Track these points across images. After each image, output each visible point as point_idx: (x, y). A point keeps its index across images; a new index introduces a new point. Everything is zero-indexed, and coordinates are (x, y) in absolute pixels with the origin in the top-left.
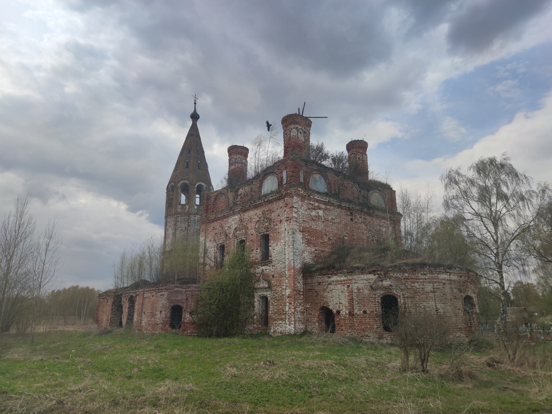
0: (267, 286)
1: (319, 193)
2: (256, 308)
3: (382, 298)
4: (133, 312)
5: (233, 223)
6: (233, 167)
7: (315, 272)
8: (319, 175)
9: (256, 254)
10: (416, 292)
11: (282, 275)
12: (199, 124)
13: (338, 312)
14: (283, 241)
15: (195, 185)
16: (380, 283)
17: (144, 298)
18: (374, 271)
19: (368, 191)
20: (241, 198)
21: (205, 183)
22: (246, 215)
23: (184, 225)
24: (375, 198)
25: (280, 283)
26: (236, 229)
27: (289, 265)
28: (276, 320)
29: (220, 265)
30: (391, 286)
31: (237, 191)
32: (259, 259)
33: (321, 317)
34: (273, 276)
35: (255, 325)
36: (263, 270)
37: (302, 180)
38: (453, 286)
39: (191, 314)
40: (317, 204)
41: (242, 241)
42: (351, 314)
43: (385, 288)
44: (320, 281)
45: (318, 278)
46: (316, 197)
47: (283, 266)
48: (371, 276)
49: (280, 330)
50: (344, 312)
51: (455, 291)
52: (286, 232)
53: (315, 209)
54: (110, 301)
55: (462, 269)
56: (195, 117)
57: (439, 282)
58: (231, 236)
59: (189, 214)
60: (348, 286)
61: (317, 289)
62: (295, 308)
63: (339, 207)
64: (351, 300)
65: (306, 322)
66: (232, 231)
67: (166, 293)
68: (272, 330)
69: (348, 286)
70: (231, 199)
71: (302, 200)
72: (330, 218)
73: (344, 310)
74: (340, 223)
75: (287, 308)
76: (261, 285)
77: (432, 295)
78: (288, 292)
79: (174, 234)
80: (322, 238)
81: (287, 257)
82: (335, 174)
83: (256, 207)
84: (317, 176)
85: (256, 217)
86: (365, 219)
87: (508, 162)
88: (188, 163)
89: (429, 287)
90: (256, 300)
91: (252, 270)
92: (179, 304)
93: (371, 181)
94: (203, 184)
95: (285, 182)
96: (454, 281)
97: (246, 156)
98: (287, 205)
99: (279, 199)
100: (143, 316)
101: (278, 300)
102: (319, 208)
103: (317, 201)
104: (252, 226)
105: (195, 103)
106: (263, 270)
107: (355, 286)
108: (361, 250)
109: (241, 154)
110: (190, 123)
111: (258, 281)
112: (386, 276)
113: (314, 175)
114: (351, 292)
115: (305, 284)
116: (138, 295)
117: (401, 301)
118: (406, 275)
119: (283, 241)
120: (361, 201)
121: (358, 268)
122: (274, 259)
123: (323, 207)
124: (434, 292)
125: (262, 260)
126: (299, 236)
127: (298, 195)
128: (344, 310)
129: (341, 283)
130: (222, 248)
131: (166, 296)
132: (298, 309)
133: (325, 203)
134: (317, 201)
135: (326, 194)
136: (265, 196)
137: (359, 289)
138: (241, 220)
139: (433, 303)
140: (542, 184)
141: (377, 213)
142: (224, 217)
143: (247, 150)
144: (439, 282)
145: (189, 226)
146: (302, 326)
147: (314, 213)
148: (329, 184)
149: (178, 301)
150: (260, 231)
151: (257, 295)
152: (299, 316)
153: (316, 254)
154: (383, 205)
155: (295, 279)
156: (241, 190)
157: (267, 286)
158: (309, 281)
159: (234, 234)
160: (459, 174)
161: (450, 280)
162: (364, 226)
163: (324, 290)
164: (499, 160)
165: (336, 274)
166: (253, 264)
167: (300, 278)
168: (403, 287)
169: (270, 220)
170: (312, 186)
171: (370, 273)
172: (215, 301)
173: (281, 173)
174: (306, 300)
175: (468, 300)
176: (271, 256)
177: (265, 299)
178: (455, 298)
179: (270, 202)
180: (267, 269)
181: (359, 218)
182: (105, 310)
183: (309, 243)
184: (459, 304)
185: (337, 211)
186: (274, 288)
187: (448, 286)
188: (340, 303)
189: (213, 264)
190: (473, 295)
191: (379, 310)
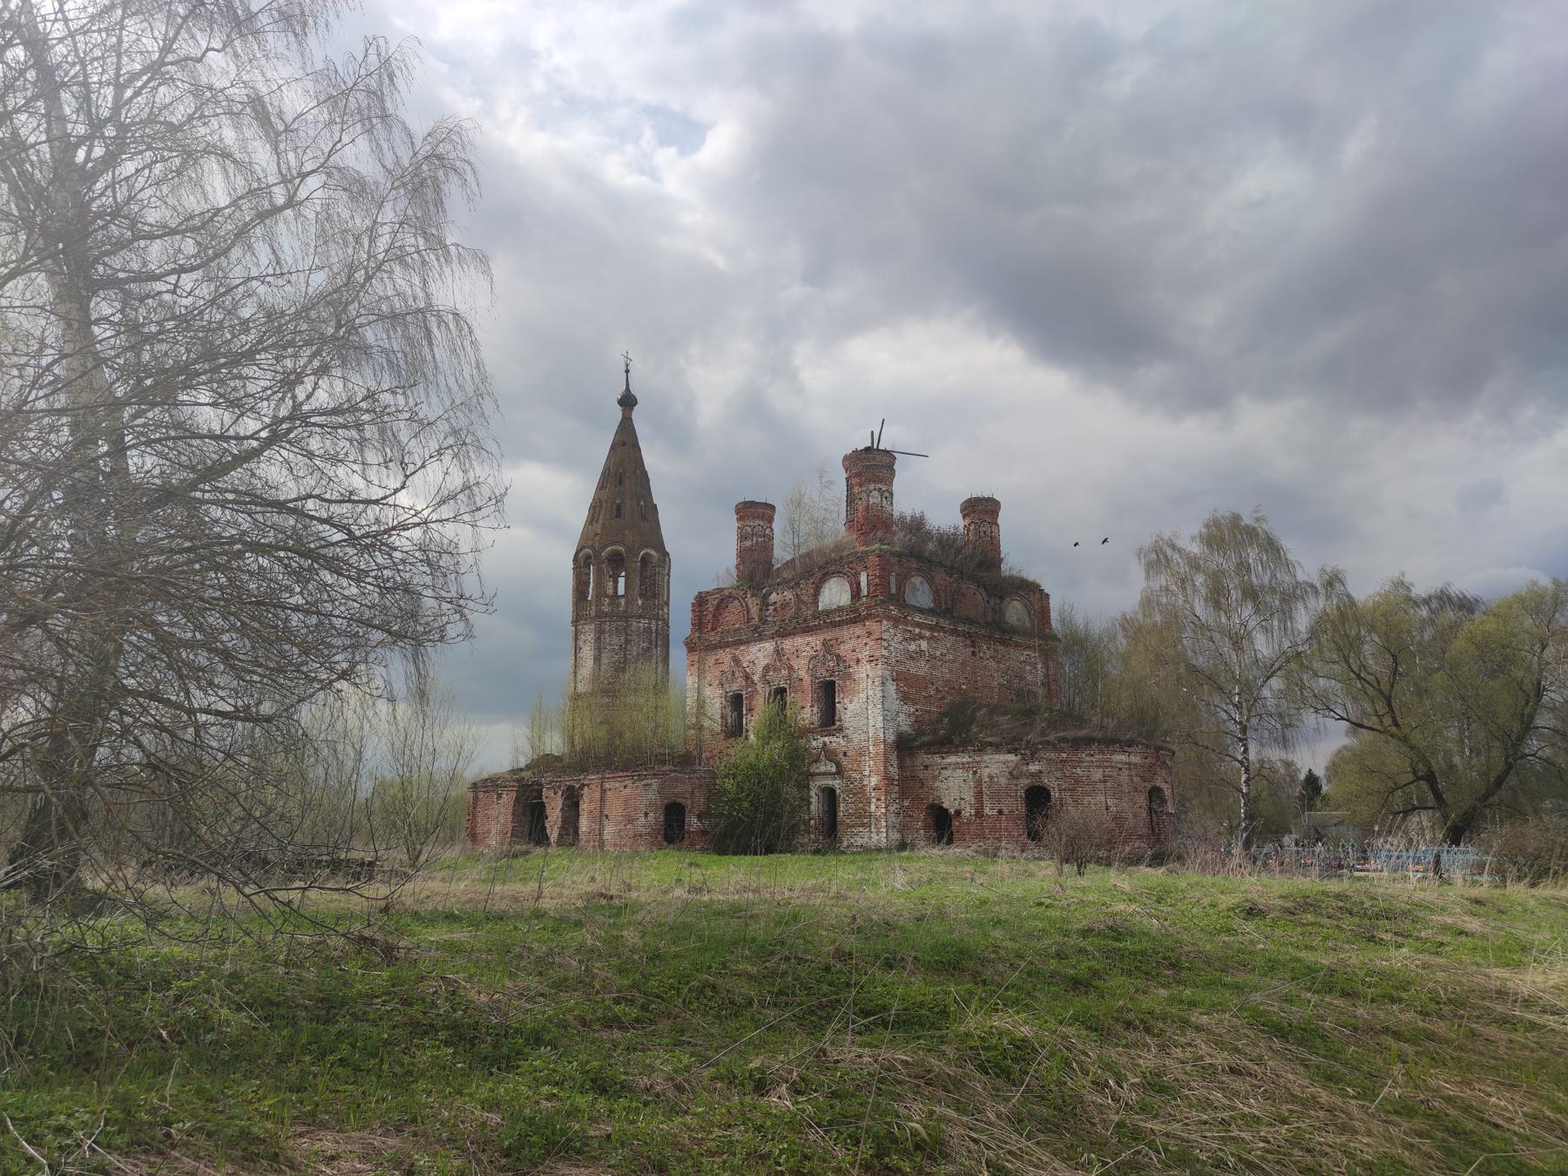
0: (834, 769)
1: (921, 611)
2: (813, 807)
3: (1026, 791)
4: (577, 815)
5: (760, 654)
6: (748, 543)
7: (919, 748)
8: (920, 579)
9: (808, 714)
10: (1077, 782)
11: (862, 753)
12: (636, 414)
13: (958, 813)
14: (863, 696)
15: (636, 555)
16: (1025, 768)
17: (603, 791)
18: (1016, 749)
19: (1002, 599)
20: (775, 610)
21: (657, 550)
22: (788, 644)
23: (617, 641)
24: (1015, 612)
25: (858, 766)
26: (767, 668)
27: (876, 739)
28: (853, 826)
29: (735, 730)
30: (1041, 772)
31: (766, 596)
32: (817, 724)
33: (930, 821)
34: (845, 754)
35: (812, 836)
36: (825, 743)
37: (893, 591)
38: (1133, 772)
39: (699, 817)
40: (917, 630)
41: (781, 692)
42: (979, 814)
43: (1032, 775)
44: (928, 763)
45: (923, 758)
46: (917, 619)
47: (863, 737)
48: (1011, 757)
49: (860, 842)
50: (968, 812)
51: (1135, 779)
52: (870, 681)
53: (914, 640)
54: (508, 799)
55: (1147, 747)
56: (628, 402)
57: (1112, 767)
58: (756, 678)
59: (626, 616)
60: (975, 772)
61: (921, 777)
62: (886, 807)
63: (954, 632)
64: (979, 795)
65: (903, 828)
66: (759, 670)
67: (655, 783)
68: (845, 843)
69: (975, 772)
70: (754, 610)
71: (895, 627)
72: (938, 654)
73: (968, 809)
74: (954, 661)
75: (873, 807)
76: (823, 769)
77: (1101, 786)
78: (874, 781)
79: (597, 659)
80: (926, 688)
81: (871, 722)
82: (946, 572)
83: (808, 630)
84: (917, 580)
85: (808, 649)
86: (996, 651)
87: (1265, 526)
88: (619, 507)
89: (1097, 774)
90: (812, 793)
91: (802, 742)
92: (679, 800)
93: (1005, 579)
94: (653, 552)
95: (865, 591)
96: (1135, 764)
97: (771, 520)
98: (869, 634)
99: (854, 621)
100: (606, 822)
101: (855, 794)
102: (922, 637)
103: (919, 625)
104: (801, 667)
105: (627, 371)
106: (825, 743)
107: (986, 772)
108: (994, 710)
109: (762, 517)
110: (617, 413)
111: (817, 761)
112: (1033, 757)
113: (913, 580)
114: (979, 783)
115: (901, 767)
116: (588, 785)
117: (1055, 794)
118: (1064, 755)
119: (863, 696)
120: (989, 619)
121: (991, 744)
122: (846, 725)
123: (928, 634)
124: (1105, 781)
125: (821, 726)
126: (891, 688)
127: (889, 618)
128: (968, 809)
129: (963, 766)
130: (736, 701)
131: (655, 786)
132: (892, 809)
133: (931, 628)
134: (919, 625)
135: (931, 612)
136: (828, 613)
137: (991, 777)
138: (779, 652)
139: (1103, 799)
140: (1329, 569)
141: (1016, 638)
142: (740, 643)
143: (773, 508)
144: (1112, 767)
145: (627, 642)
146: (897, 836)
147: (913, 647)
148: (936, 593)
149: (677, 795)
150: (818, 675)
151: (816, 785)
152: (892, 819)
153: (917, 716)
154: (1028, 625)
155: (886, 760)
156: (774, 595)
157: (834, 769)
158: (908, 762)
159: (764, 676)
160: (1173, 547)
161: (1129, 764)
162: (994, 664)
163: (935, 778)
164: (1247, 520)
165: (955, 753)
166: (806, 732)
167: (893, 757)
168: (1059, 774)
169: (838, 656)
170: (910, 599)
171: (1009, 752)
172: (748, 796)
173: (857, 574)
174: (903, 794)
175: (1155, 794)
176: (840, 720)
177: (830, 795)
178: (1136, 790)
179: (835, 625)
180: (835, 742)
181: (985, 649)
182: (493, 813)
183: (905, 698)
184: (1142, 800)
185: (950, 640)
186: (846, 774)
187: (1125, 773)
188: (962, 799)
189: (718, 729)
190: (1164, 786)
191: (1022, 808)
